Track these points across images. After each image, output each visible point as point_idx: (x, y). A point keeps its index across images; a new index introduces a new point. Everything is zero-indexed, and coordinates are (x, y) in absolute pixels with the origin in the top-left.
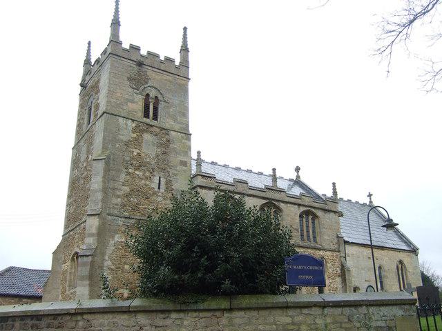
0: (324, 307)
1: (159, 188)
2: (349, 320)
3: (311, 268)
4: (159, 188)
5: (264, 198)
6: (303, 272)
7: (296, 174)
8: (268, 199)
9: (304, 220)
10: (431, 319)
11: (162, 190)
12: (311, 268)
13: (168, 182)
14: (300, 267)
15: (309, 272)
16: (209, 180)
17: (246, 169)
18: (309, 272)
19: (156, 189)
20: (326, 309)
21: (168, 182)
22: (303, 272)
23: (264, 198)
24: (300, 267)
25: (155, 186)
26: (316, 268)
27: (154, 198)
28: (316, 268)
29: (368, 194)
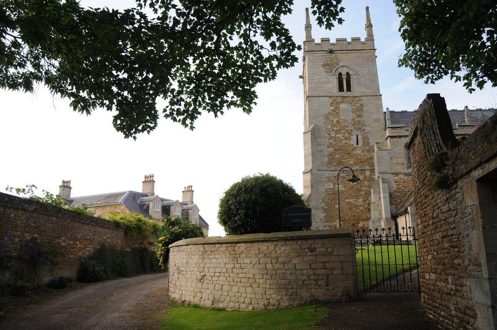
1: (357, 144)
4: (357, 144)
11: (360, 145)
19: (355, 145)
21: (365, 138)
24: (301, 214)
25: (353, 141)
26: (305, 214)
27: (355, 152)
28: (305, 214)
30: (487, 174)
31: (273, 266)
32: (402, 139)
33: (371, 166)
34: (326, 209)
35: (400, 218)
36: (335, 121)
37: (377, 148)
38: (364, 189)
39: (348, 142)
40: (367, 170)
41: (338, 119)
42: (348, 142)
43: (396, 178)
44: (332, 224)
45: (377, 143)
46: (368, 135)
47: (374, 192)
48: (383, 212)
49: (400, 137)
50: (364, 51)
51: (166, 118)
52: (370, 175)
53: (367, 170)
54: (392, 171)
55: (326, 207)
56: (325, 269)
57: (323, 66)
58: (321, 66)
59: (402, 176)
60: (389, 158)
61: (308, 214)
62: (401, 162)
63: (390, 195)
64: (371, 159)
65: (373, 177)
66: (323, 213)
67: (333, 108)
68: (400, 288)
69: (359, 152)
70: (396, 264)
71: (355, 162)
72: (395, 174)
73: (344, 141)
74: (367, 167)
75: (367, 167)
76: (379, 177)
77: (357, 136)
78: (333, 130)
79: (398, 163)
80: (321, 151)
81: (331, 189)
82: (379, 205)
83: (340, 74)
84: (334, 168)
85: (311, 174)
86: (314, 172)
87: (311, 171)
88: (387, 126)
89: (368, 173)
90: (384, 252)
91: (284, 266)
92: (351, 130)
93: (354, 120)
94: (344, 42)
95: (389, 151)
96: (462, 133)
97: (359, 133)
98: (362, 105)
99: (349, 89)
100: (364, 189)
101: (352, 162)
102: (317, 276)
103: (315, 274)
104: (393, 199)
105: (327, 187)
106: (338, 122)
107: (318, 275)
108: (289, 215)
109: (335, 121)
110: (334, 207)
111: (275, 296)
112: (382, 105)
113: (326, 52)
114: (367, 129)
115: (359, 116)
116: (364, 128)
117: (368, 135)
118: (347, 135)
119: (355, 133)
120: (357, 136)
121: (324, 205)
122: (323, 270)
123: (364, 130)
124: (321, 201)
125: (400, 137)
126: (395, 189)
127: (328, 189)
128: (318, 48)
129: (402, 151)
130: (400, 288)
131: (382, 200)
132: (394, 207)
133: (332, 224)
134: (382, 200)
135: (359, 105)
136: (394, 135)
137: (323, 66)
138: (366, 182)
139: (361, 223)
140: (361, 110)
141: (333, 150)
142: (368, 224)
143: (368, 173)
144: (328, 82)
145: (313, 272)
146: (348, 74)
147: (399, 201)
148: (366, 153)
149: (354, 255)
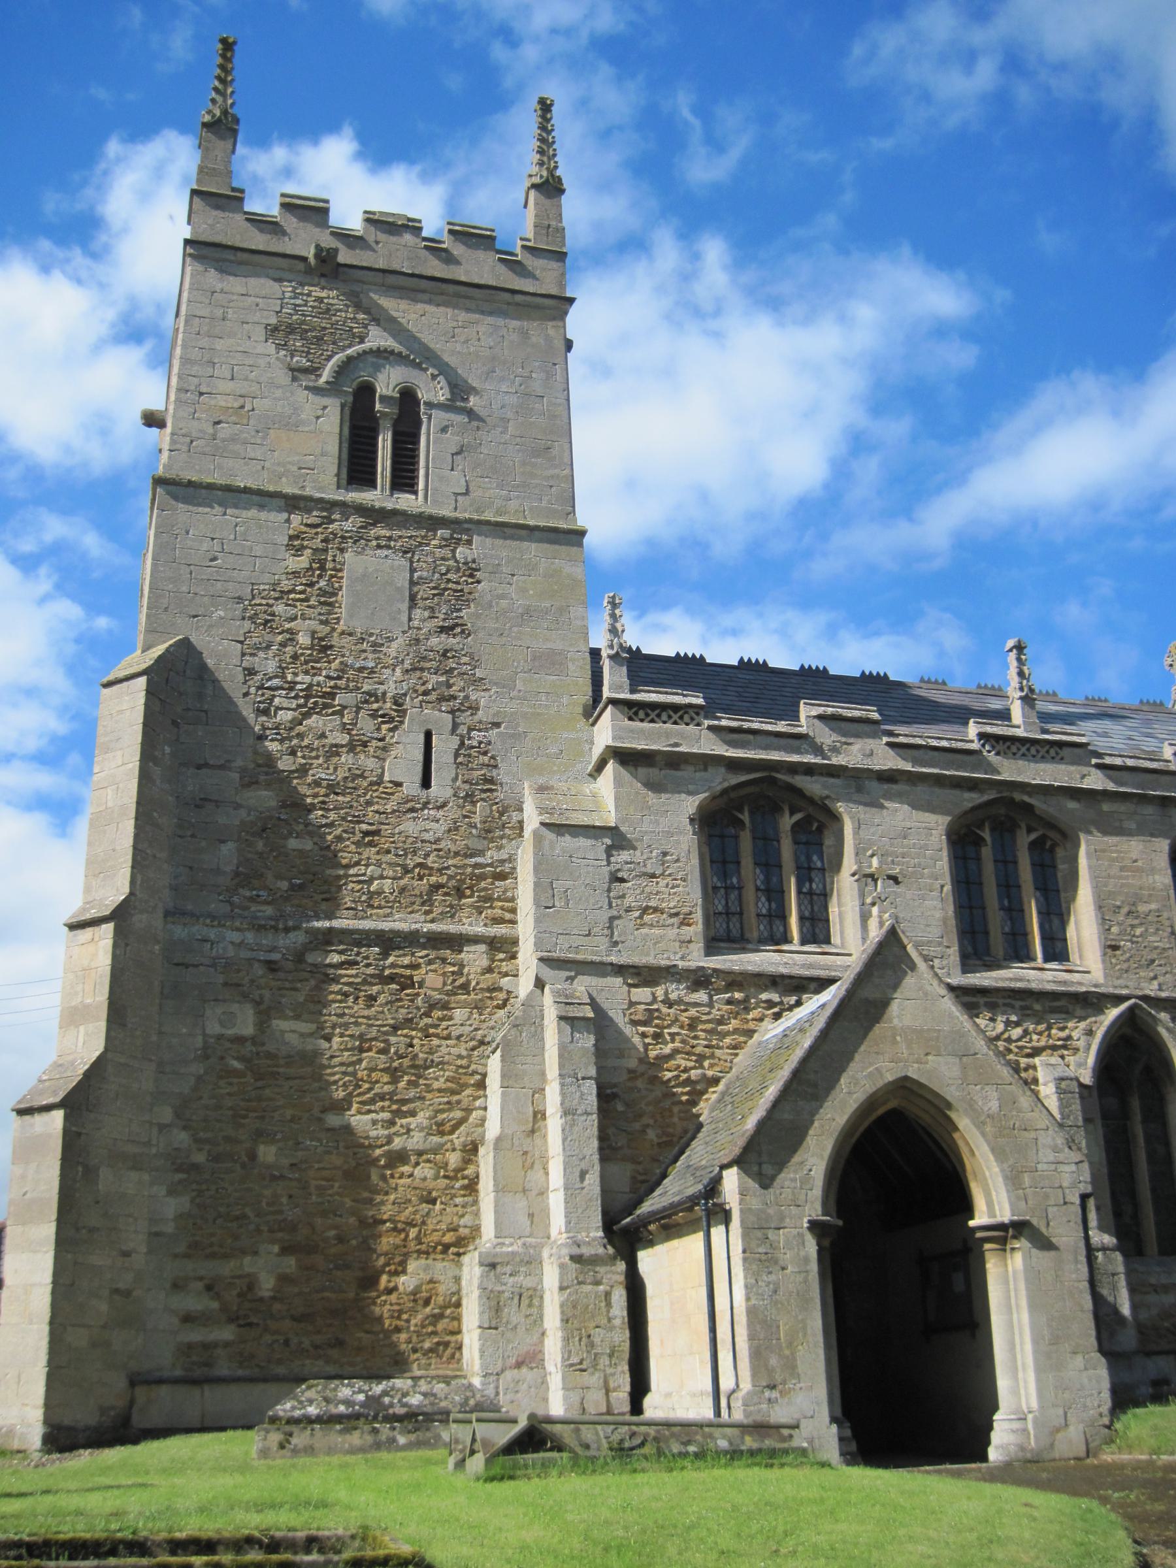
1: (426, 783)
4: (426, 783)
11: (440, 789)
19: (412, 786)
23: (973, 785)
30: (838, 1080)
33: (498, 921)
34: (195, 1167)
35: (661, 1250)
36: (303, 639)
37: (542, 810)
40: (475, 940)
41: (323, 630)
43: (642, 994)
44: (226, 1269)
47: (504, 1076)
48: (556, 1202)
50: (507, 296)
55: (200, 1158)
57: (272, 331)
58: (260, 333)
63: (605, 1097)
64: (502, 876)
65: (505, 982)
66: (170, 1193)
67: (303, 562)
73: (345, 759)
76: (540, 984)
77: (428, 735)
78: (292, 686)
80: (201, 803)
81: (240, 1040)
82: (447, 1369)
83: (365, 392)
84: (269, 910)
85: (118, 934)
86: (139, 920)
87: (120, 915)
88: (606, 693)
94: (408, 237)
97: (440, 719)
99: (404, 479)
105: (214, 1028)
106: (323, 647)
109: (303, 639)
110: (253, 1156)
113: (301, 266)
118: (366, 725)
119: (418, 716)
120: (428, 735)
121: (182, 1138)
124: (166, 1114)
127: (220, 1037)
128: (258, 240)
131: (554, 1125)
133: (226, 1269)
134: (554, 1125)
137: (272, 331)
139: (412, 1266)
141: (273, 803)
142: (457, 1280)
144: (290, 424)
146: (407, 398)
149: (597, 1040)
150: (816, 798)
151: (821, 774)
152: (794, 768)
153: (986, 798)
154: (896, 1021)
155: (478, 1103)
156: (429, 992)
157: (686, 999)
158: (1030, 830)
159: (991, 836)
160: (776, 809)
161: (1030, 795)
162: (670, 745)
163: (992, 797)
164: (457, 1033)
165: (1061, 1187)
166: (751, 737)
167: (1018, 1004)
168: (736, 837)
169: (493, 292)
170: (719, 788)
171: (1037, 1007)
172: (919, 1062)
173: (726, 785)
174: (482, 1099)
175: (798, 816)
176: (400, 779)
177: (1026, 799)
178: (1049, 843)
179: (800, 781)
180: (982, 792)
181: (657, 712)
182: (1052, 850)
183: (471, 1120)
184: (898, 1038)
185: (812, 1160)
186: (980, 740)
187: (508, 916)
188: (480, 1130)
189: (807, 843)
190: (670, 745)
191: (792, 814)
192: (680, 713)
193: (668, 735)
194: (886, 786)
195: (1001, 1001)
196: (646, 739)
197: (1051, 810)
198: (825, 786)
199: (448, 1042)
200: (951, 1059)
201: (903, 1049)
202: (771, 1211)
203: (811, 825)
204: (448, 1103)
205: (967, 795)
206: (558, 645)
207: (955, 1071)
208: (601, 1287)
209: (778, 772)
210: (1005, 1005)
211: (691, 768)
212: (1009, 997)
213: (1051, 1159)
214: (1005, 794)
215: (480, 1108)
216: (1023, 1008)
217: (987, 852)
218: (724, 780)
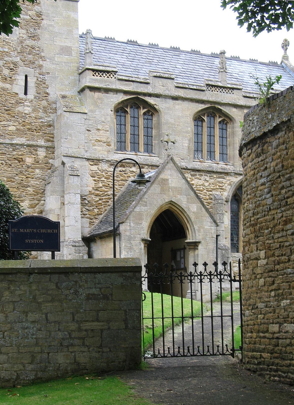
0: (31, 274)
1: (26, 93)
2: (57, 286)
3: (43, 231)
4: (26, 93)
5: (202, 102)
6: (32, 236)
7: (282, 52)
8: (208, 102)
9: (205, 130)
10: (167, 297)
11: (31, 96)
12: (43, 231)
13: (41, 83)
14: (28, 231)
15: (40, 236)
16: (105, 77)
17: (209, 53)
18: (40, 236)
19: (22, 95)
20: (32, 276)
21: (41, 83)
22: (32, 236)
23: (202, 102)
24: (28, 231)
25: (19, 88)
26: (49, 231)
27: (20, 109)
28: (49, 231)
29: (207, 263)
31: (7, 317)
32: (111, 95)
33: (49, 141)
38: (32, 182)
39: (8, 86)
40: (41, 147)
42: (8, 86)
43: (95, 168)
45: (64, 97)
46: (46, 77)
49: (107, 91)
51: (270, 61)
52: (46, 157)
53: (41, 147)
54: (87, 155)
56: (98, 320)
59: (104, 166)
60: (83, 128)
61: (55, 231)
62: (104, 139)
68: (186, 351)
69: (28, 110)
70: (173, 318)
71: (17, 129)
72: (93, 160)
74: (41, 142)
75: (41, 142)
77: (26, 77)
79: (99, 141)
89: (42, 153)
90: (204, 295)
91: (27, 316)
92: (15, 64)
93: (22, 42)
95: (85, 116)
96: (211, 99)
97: (30, 71)
98: (39, 15)
100: (32, 182)
101: (12, 128)
102: (84, 333)
103: (80, 329)
104: (87, 207)
107: (86, 330)
108: (21, 230)
111: (10, 365)
112: (76, 21)
114: (47, 65)
115: (33, 37)
116: (41, 63)
117: (46, 77)
119: (22, 70)
120: (26, 77)
122: (96, 323)
123: (41, 67)
125: (107, 91)
126: (91, 189)
129: (109, 119)
130: (186, 351)
132: (87, 221)
135: (34, 13)
136: (97, 85)
138: (37, 171)
140: (38, 25)
143: (42, 153)
145: (77, 326)
147: (96, 210)
148: (41, 114)
150: (152, 105)
151: (154, 97)
152: (145, 94)
153: (206, 106)
154: (170, 185)
155: (42, 199)
156: (27, 164)
157: (108, 170)
158: (220, 117)
159: (207, 118)
160: (138, 108)
161: (221, 106)
162: (106, 85)
163: (208, 106)
164: (36, 177)
165: (211, 233)
166: (132, 83)
167: (209, 175)
168: (125, 116)
169: (194, 326)
170: (121, 100)
171: (215, 176)
172: (175, 197)
173: (123, 99)
174: (44, 198)
175: (145, 110)
176: (17, 92)
177: (219, 107)
178: (225, 122)
179: (148, 99)
180: (205, 104)
181: (102, 73)
182: (226, 124)
183: (40, 204)
184: (170, 190)
185: (144, 223)
186: (207, 86)
187: (51, 139)
188: (43, 207)
189: (147, 119)
190: (106, 85)
191: (143, 109)
192: (109, 74)
193: (106, 82)
194: (174, 101)
195: (203, 174)
196: (98, 83)
197: (227, 112)
198: (155, 101)
199: (33, 180)
200: (184, 196)
201: (171, 193)
202: (132, 236)
203: (149, 113)
204: (33, 198)
205: (200, 105)
206: (69, 45)
207: (185, 200)
208: (81, 254)
209: (140, 95)
210: (204, 175)
211: (112, 93)
212: (206, 173)
213: (209, 225)
214: (213, 106)
215: (43, 200)
216: (210, 177)
217: (205, 125)
218: (122, 98)
